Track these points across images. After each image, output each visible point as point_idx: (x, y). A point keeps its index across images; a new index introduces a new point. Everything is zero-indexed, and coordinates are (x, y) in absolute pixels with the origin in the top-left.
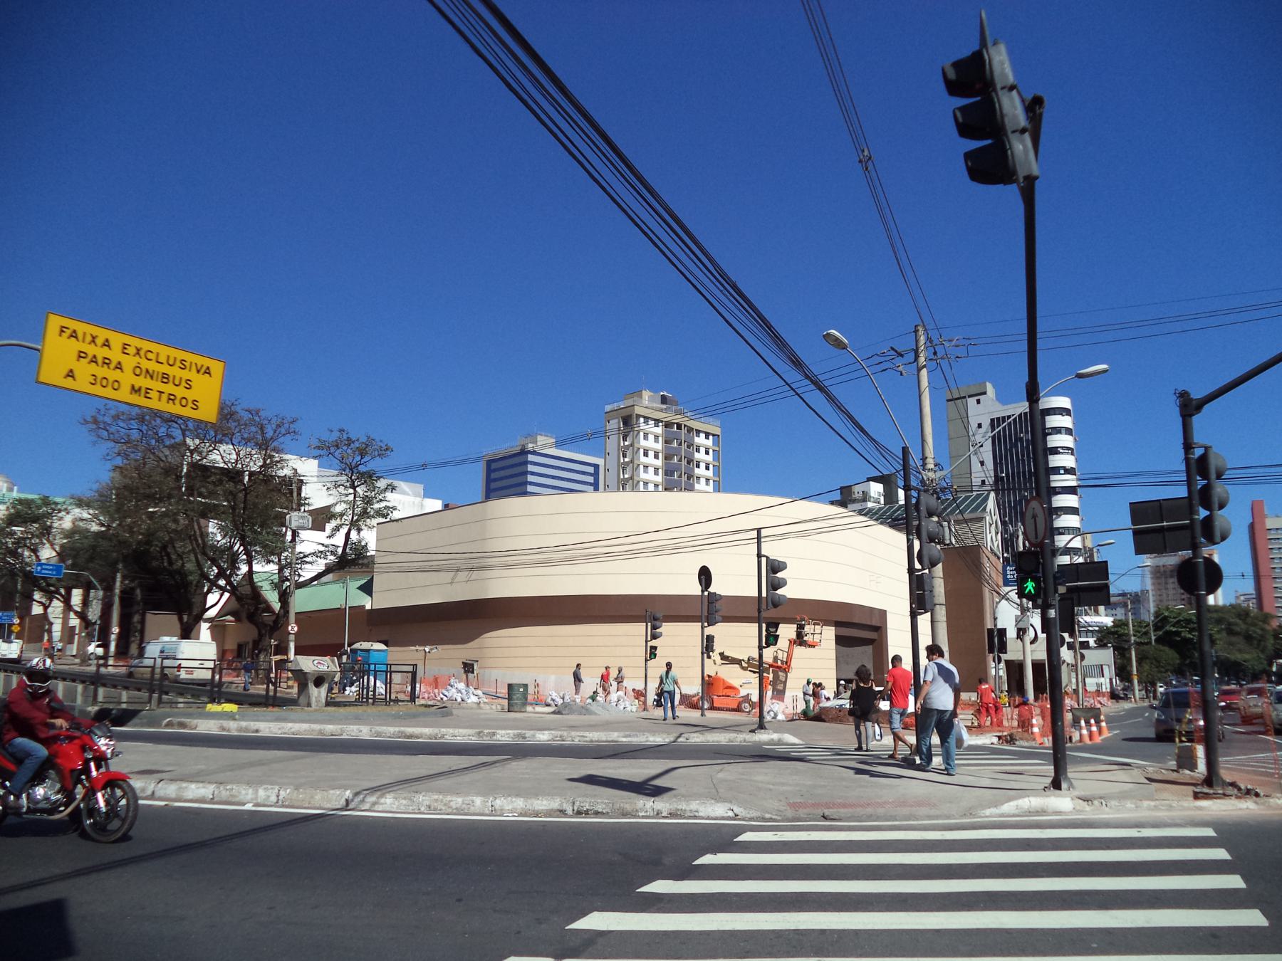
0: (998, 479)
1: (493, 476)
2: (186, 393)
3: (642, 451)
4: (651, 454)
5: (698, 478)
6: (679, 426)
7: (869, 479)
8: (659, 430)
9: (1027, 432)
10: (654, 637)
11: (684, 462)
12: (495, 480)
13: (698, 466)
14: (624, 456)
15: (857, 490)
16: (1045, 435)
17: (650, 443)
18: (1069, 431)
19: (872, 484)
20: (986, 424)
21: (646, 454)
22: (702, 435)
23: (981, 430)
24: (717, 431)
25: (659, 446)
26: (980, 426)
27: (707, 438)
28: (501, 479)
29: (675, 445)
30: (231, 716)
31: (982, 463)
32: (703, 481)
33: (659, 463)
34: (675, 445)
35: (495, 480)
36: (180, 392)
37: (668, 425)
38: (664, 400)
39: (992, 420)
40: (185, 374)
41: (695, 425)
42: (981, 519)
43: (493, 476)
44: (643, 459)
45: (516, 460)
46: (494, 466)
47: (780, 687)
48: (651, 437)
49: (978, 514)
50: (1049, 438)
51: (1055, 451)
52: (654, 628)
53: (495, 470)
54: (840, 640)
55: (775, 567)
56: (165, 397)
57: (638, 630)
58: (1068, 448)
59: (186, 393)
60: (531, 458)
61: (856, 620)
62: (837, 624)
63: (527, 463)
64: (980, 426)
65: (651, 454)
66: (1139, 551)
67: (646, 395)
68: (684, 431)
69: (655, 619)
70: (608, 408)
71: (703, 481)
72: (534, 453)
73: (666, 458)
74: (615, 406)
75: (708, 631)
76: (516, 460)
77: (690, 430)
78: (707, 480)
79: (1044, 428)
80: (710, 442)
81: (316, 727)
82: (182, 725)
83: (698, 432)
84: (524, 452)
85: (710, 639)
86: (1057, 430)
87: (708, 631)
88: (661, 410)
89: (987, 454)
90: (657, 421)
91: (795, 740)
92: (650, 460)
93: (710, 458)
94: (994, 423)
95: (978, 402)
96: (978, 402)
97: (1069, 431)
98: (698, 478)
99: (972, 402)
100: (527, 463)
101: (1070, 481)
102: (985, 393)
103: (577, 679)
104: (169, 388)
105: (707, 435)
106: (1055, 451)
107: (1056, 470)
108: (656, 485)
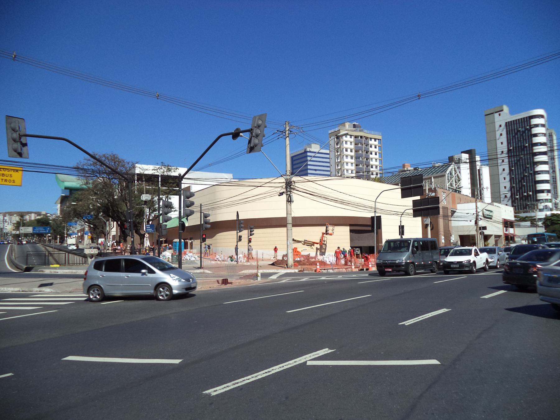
0: (509, 151)
1: (294, 163)
2: (10, 178)
3: (344, 150)
4: (349, 150)
5: (372, 159)
6: (361, 137)
7: (462, 152)
8: (352, 139)
9: (522, 128)
10: (251, 235)
11: (364, 153)
12: (295, 164)
13: (371, 154)
14: (337, 152)
15: (456, 157)
16: (531, 128)
17: (348, 146)
18: (543, 126)
19: (463, 154)
20: (503, 125)
21: (346, 151)
22: (373, 140)
23: (501, 128)
24: (380, 137)
25: (352, 146)
26: (500, 126)
27: (351, 137)
28: (297, 164)
29: (360, 145)
30: (55, 268)
31: (502, 143)
32: (374, 160)
33: (353, 154)
34: (360, 145)
35: (295, 164)
36: (8, 178)
37: (356, 137)
38: (354, 126)
39: (506, 123)
40: (10, 173)
41: (369, 136)
42: (444, 175)
43: (294, 163)
44: (345, 153)
45: (303, 155)
46: (294, 158)
47: (323, 251)
48: (349, 143)
49: (443, 174)
50: (533, 129)
51: (536, 135)
52: (251, 232)
53: (295, 160)
54: (351, 231)
55: (206, 216)
56: (4, 181)
57: (370, 224)
58: (543, 134)
59: (10, 178)
60: (309, 154)
61: (360, 223)
62: (350, 225)
63: (307, 156)
64: (500, 126)
65: (349, 150)
66: (404, 196)
67: (347, 125)
68: (364, 139)
69: (251, 228)
70: (330, 132)
71: (374, 160)
72: (310, 152)
73: (356, 151)
74: (333, 131)
75: (240, 234)
76: (303, 155)
77: (367, 138)
78: (376, 160)
79: (530, 125)
80: (377, 143)
81: (71, 271)
82: (42, 271)
83: (371, 139)
84: (306, 152)
85: (240, 237)
86: (537, 126)
87: (240, 234)
88: (352, 131)
89: (504, 139)
90: (351, 136)
91: (209, 272)
92: (349, 153)
93: (377, 150)
94: (508, 124)
95: (500, 115)
96: (500, 115)
97: (543, 126)
98: (372, 159)
99: (496, 115)
100: (307, 156)
101: (543, 149)
102: (502, 111)
103: (276, 249)
104: (5, 178)
105: (375, 140)
106: (536, 135)
107: (536, 144)
108: (352, 164)
